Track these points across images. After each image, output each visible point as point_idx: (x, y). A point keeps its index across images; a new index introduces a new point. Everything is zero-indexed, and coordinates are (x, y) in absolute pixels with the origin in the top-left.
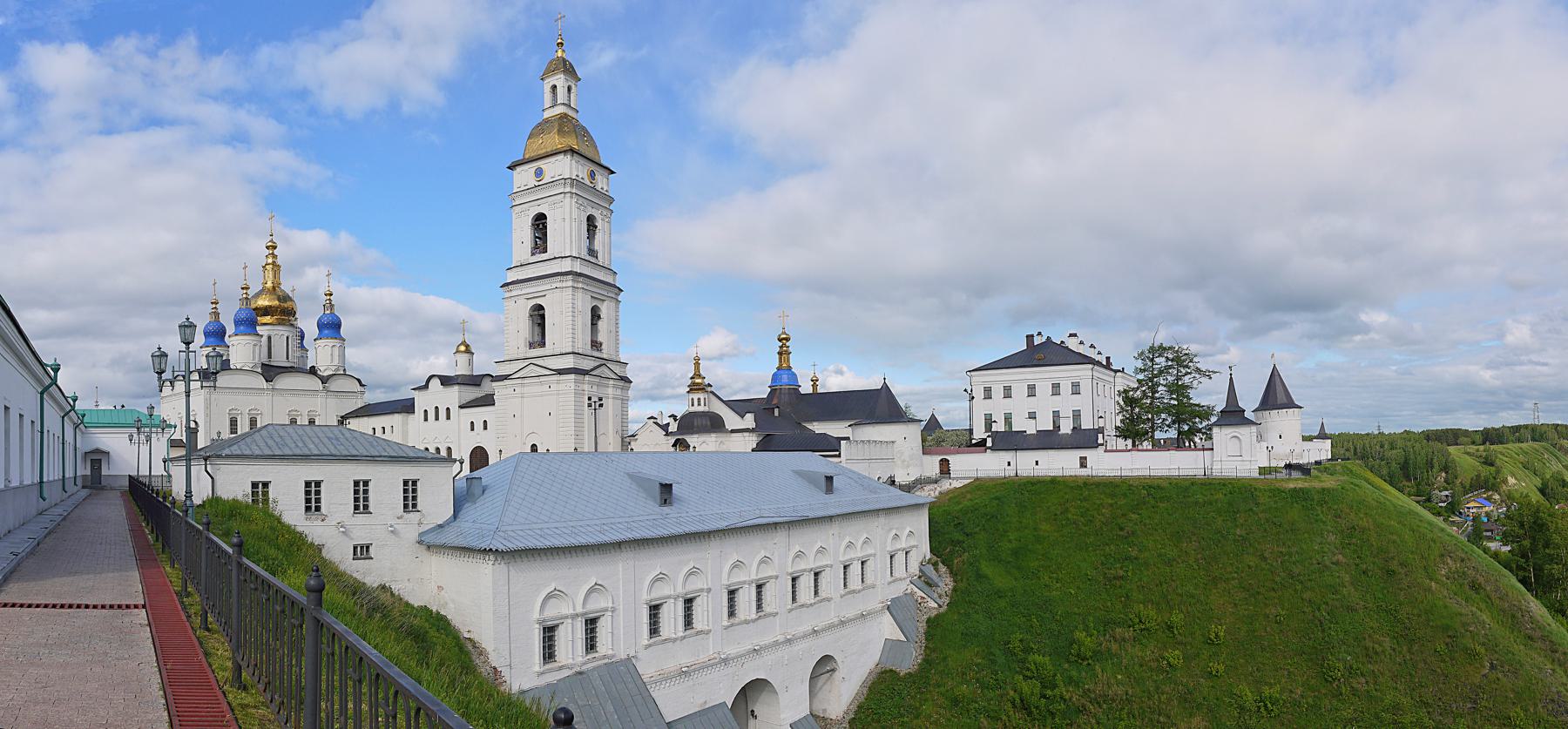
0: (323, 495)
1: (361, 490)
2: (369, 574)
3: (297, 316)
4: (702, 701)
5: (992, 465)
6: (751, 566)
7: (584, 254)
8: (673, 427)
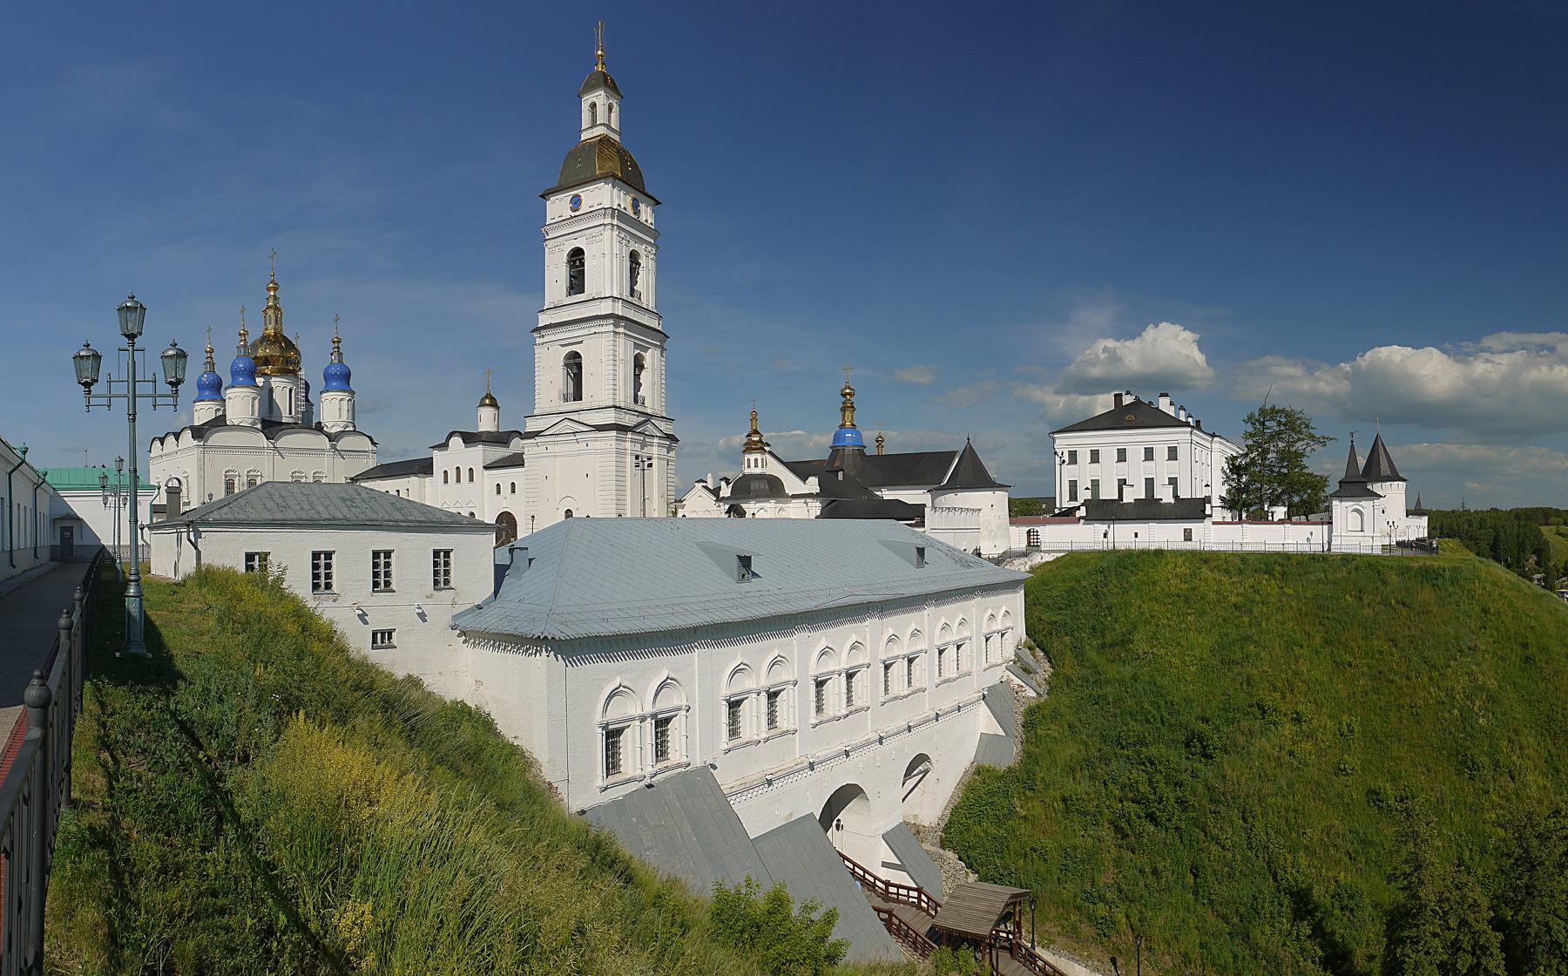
0: (334, 570)
1: (382, 562)
2: (395, 663)
3: (301, 366)
5: (1086, 536)
6: (841, 653)
7: (626, 295)
8: (726, 491)
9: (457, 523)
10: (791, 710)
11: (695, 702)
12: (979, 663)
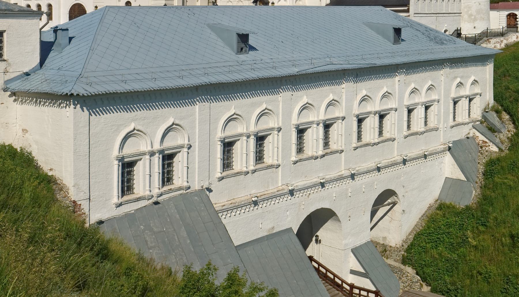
4: (270, 226)
9: (9, 10)
10: (276, 149)
11: (195, 142)
12: (446, 121)
